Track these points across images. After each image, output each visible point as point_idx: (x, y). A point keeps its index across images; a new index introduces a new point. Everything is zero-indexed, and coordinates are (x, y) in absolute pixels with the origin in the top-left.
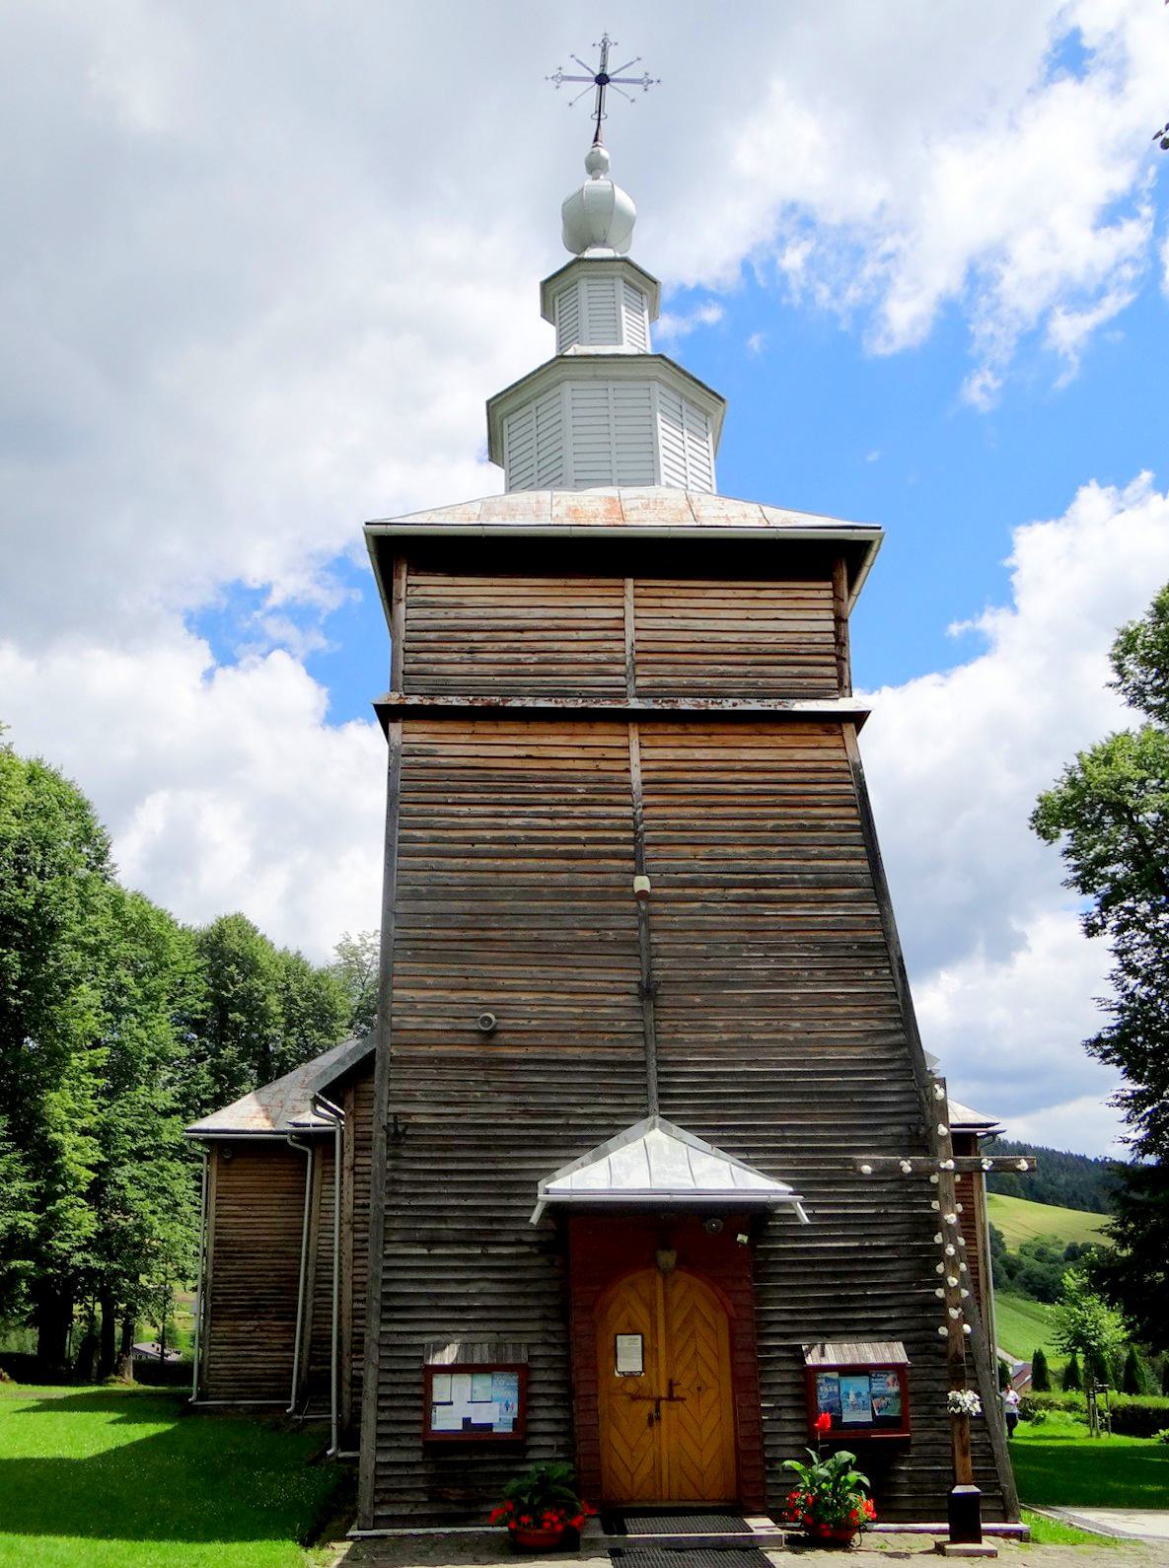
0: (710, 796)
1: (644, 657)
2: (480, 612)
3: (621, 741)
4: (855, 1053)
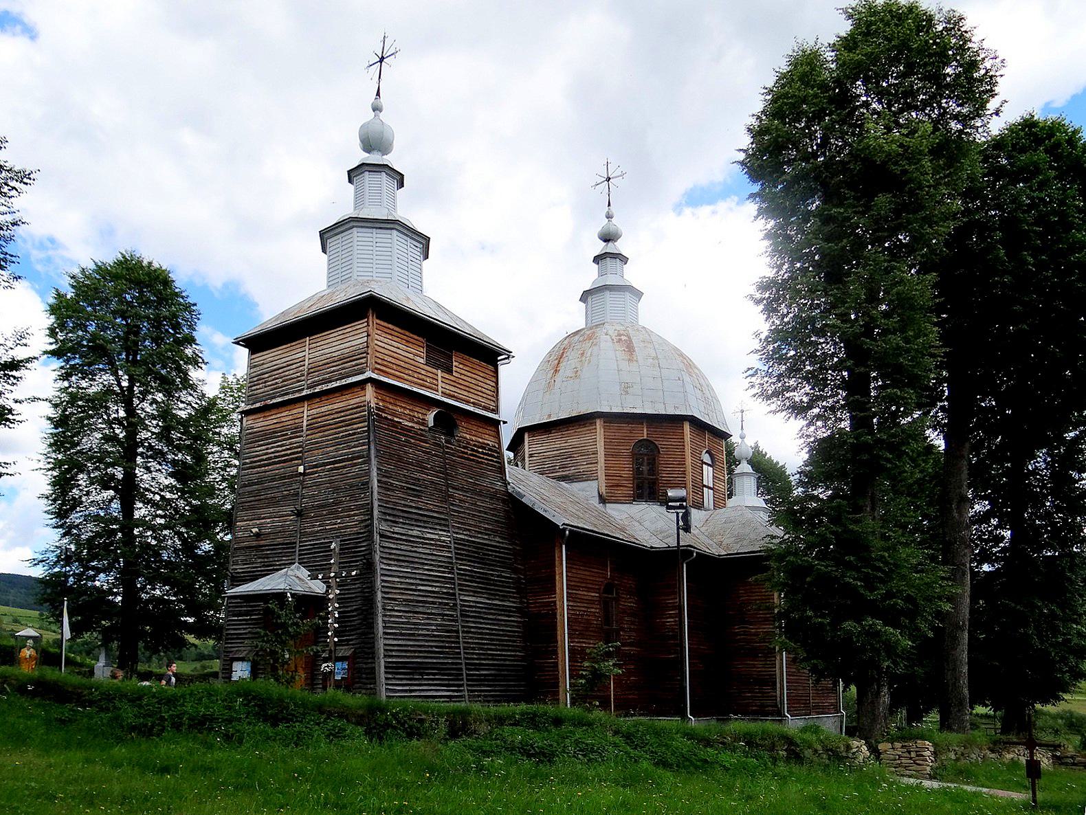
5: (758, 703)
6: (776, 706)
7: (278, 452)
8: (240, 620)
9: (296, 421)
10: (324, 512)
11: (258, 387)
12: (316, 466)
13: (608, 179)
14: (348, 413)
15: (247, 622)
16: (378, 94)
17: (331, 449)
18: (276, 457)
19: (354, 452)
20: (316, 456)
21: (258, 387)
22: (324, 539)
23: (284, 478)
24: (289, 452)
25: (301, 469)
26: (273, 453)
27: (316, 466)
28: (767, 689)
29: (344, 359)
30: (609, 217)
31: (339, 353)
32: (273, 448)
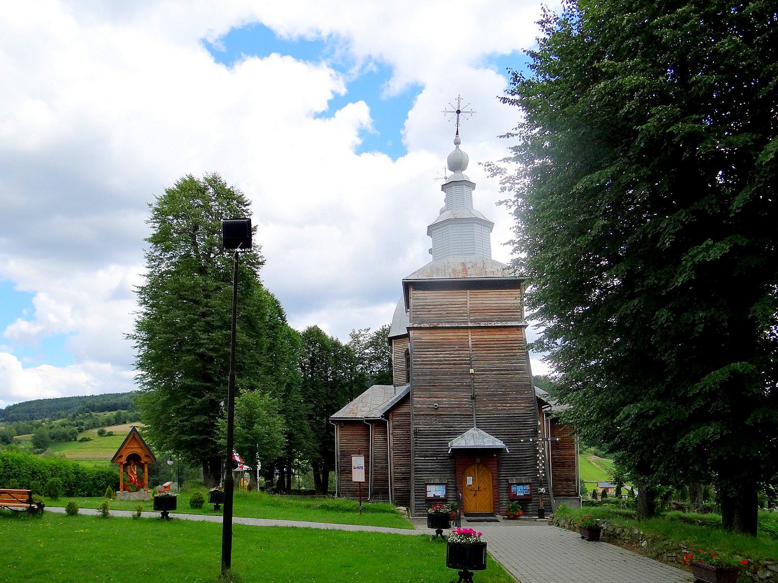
0: (488, 348)
1: (474, 311)
2: (431, 300)
3: (466, 334)
4: (522, 411)
5: (565, 490)
6: (575, 492)
7: (456, 360)
8: (427, 460)
9: (462, 340)
10: (496, 399)
11: (423, 313)
12: (484, 371)
13: (458, 112)
14: (508, 342)
15: (434, 461)
16: (457, 134)
17: (496, 362)
18: (445, 360)
19: (515, 366)
20: (483, 365)
21: (423, 313)
22: (497, 414)
23: (456, 374)
24: (457, 359)
25: (472, 371)
26: (442, 357)
27: (484, 371)
28: (570, 483)
29: (508, 310)
30: (457, 143)
31: (497, 305)
32: (443, 354)
